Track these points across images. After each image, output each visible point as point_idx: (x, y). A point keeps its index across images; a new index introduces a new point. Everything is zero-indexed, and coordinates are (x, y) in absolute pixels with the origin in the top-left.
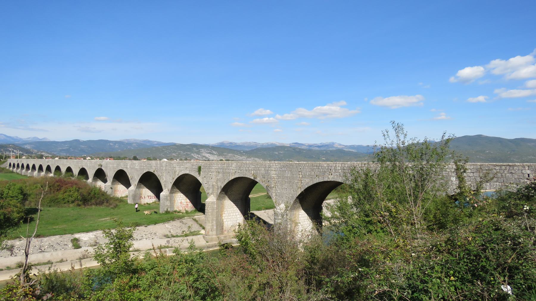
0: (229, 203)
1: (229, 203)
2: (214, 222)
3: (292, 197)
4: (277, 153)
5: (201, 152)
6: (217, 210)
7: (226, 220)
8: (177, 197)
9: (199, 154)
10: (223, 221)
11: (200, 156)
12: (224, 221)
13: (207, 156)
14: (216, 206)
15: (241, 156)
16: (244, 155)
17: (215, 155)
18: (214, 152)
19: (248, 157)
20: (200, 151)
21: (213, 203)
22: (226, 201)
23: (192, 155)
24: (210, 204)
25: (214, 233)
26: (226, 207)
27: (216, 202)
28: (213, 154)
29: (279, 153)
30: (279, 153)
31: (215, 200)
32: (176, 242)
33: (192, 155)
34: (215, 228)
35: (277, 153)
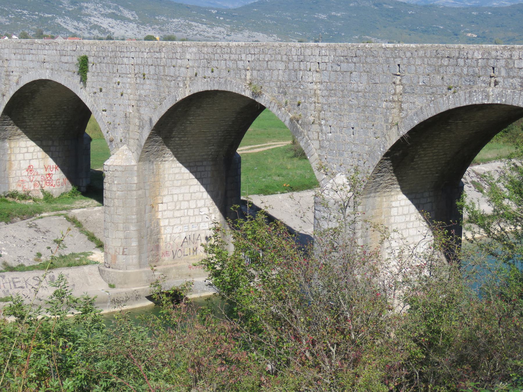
0: (177, 170)
1: (177, 170)
2: (133, 228)
3: (371, 153)
4: (323, 16)
5: (83, 12)
6: (140, 192)
7: (166, 222)
8: (17, 151)
9: (78, 20)
10: (158, 224)
11: (81, 25)
12: (162, 224)
13: (105, 26)
14: (135, 180)
15: (212, 26)
16: (219, 23)
17: (130, 21)
18: (127, 14)
19: (232, 30)
20: (81, 8)
21: (126, 169)
22: (167, 165)
23: (59, 20)
24: (117, 174)
25: (133, 259)
26: (168, 184)
27: (135, 168)
28: (123, 19)
29: (330, 17)
30: (330, 17)
31: (134, 163)
32: (18, 285)
33: (59, 20)
34: (134, 244)
35: (323, 16)
